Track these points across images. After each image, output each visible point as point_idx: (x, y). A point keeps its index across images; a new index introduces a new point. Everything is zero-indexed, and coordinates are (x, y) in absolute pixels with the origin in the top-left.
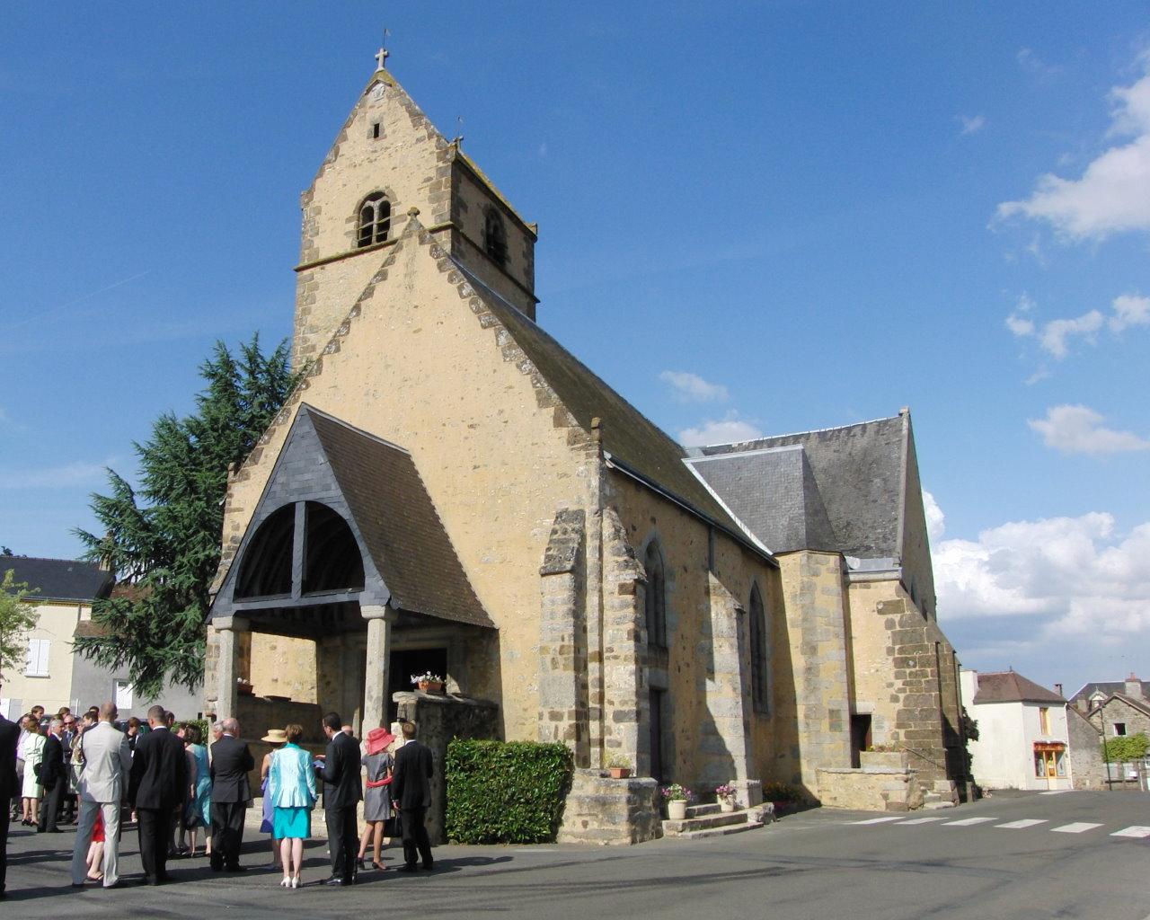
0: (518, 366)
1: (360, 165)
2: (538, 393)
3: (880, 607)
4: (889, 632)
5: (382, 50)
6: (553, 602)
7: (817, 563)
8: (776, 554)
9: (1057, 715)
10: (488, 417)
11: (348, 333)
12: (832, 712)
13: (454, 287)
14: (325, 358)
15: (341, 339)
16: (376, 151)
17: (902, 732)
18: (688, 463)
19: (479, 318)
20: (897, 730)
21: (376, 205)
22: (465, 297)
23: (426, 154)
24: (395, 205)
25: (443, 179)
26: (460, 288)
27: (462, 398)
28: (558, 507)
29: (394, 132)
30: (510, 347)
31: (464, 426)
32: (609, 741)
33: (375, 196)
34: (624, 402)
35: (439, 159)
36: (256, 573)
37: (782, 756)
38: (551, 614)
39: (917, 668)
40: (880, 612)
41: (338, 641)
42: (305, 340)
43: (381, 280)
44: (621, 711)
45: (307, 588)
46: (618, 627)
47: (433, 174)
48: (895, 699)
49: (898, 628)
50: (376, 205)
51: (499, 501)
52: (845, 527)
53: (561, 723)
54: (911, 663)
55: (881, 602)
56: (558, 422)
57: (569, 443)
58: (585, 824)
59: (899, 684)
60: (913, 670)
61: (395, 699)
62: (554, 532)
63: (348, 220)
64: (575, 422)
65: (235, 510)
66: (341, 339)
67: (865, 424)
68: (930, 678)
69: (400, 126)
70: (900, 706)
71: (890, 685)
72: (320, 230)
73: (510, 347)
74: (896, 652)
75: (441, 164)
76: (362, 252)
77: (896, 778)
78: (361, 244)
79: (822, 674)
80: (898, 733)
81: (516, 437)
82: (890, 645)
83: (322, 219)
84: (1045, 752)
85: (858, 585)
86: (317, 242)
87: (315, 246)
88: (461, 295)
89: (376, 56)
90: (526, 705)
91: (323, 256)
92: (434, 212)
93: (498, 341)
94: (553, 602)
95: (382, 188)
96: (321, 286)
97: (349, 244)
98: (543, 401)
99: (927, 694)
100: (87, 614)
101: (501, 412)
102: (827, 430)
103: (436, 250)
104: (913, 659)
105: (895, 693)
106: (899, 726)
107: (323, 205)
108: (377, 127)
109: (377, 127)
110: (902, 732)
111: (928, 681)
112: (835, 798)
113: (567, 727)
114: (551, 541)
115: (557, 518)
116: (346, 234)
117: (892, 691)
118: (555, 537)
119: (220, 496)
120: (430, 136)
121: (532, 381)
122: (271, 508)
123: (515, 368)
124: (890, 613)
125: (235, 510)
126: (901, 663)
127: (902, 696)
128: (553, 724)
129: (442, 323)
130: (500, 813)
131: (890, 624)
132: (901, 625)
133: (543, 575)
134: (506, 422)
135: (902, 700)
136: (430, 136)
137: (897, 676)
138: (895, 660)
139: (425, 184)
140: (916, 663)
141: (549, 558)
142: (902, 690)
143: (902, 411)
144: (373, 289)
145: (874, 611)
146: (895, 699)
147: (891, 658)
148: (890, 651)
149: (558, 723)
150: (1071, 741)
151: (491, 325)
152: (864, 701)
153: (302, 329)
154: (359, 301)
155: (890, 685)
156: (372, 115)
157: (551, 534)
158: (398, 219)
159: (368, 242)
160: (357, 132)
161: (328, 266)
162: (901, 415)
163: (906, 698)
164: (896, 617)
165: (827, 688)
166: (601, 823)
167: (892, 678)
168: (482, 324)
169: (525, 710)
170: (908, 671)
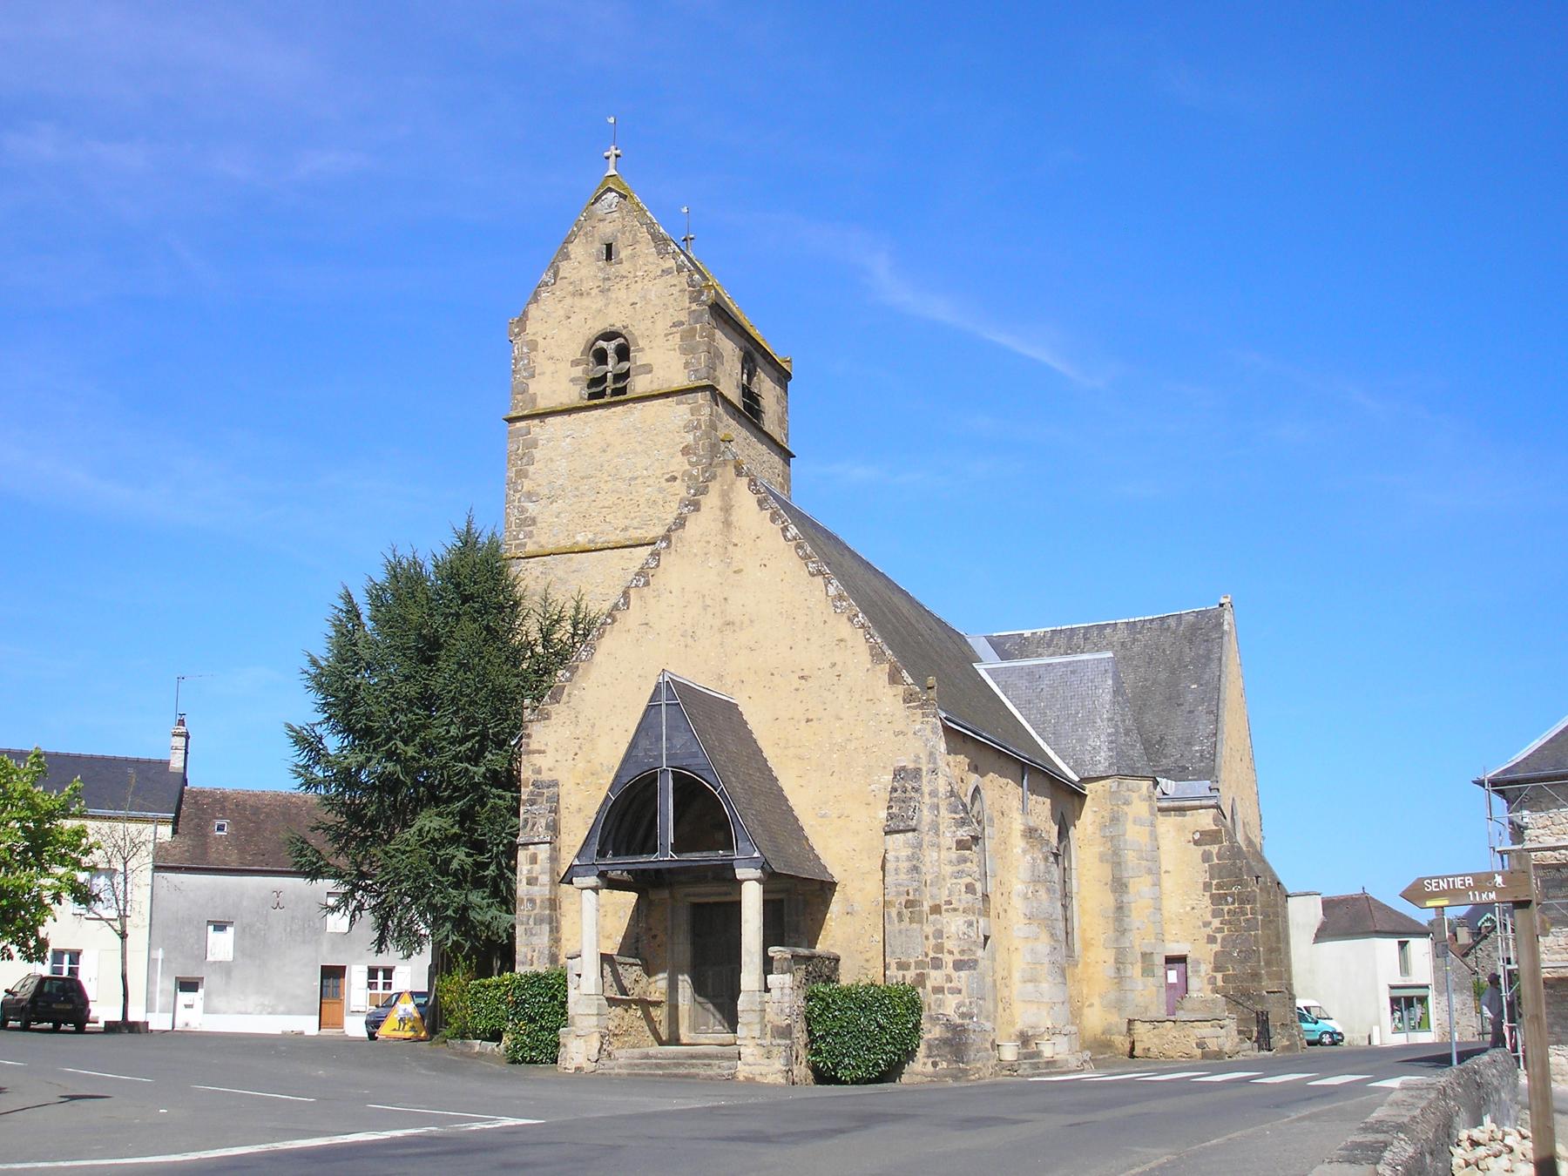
0: (849, 619)
1: (588, 294)
2: (872, 648)
3: (1197, 836)
4: (1207, 865)
5: (613, 147)
6: (897, 859)
7: (1128, 790)
8: (1085, 780)
9: (1420, 948)
10: (819, 669)
11: (658, 566)
12: (1144, 955)
13: (778, 527)
14: (632, 592)
15: (651, 572)
16: (609, 279)
17: (1219, 976)
18: (981, 669)
19: (806, 565)
20: (1215, 974)
21: (610, 347)
22: (789, 540)
23: (675, 291)
24: (634, 351)
25: (698, 326)
26: (784, 530)
27: (791, 648)
28: (896, 765)
29: (633, 256)
30: (840, 597)
31: (795, 677)
32: (949, 988)
33: (609, 336)
34: (918, 606)
35: (693, 299)
36: (725, 860)
37: (1091, 1005)
38: (896, 870)
39: (1236, 905)
40: (1196, 843)
41: (666, 894)
42: (523, 510)
43: (693, 511)
44: (961, 960)
45: (677, 848)
46: (955, 881)
47: (684, 317)
48: (1211, 939)
49: (1216, 861)
50: (610, 347)
51: (835, 756)
52: (1159, 742)
53: (909, 972)
54: (1230, 899)
55: (1197, 831)
56: (894, 678)
57: (904, 701)
58: (935, 1064)
59: (1216, 923)
60: (1231, 907)
61: (770, 954)
62: (894, 790)
63: (575, 363)
64: (910, 681)
65: (534, 752)
66: (651, 572)
67: (1181, 614)
68: (1250, 916)
69: (640, 256)
70: (1217, 947)
71: (1207, 924)
72: (537, 372)
73: (840, 597)
74: (1214, 887)
75: (694, 306)
76: (596, 407)
77: (1212, 1026)
78: (592, 396)
79: (1134, 914)
80: (1215, 978)
81: (850, 692)
82: (1207, 880)
83: (539, 358)
84: (1406, 1003)
85: (1173, 813)
86: (534, 387)
87: (531, 391)
88: (785, 537)
89: (606, 154)
90: (868, 956)
91: (543, 404)
92: (686, 365)
93: (827, 591)
94: (897, 859)
95: (618, 326)
96: (540, 442)
97: (574, 394)
98: (877, 656)
99: (1246, 933)
100: (165, 832)
101: (834, 665)
102: (1137, 619)
103: (755, 485)
104: (1232, 895)
105: (1211, 933)
106: (1217, 969)
107: (540, 340)
108: (609, 247)
109: (609, 247)
110: (1219, 976)
111: (1248, 920)
112: (1149, 1049)
113: (914, 976)
114: (891, 800)
115: (895, 775)
116: (572, 380)
117: (1209, 931)
118: (895, 795)
119: (512, 735)
120: (680, 269)
121: (865, 636)
122: (634, 772)
123: (846, 620)
124: (1206, 844)
125: (534, 752)
126: (1217, 900)
127: (1219, 936)
128: (901, 972)
129: (765, 565)
130: (880, 1045)
131: (1206, 857)
132: (1219, 859)
133: (886, 833)
134: (839, 676)
135: (1219, 940)
136: (680, 269)
137: (1215, 914)
138: (1212, 896)
139: (674, 329)
140: (1234, 899)
141: (891, 817)
142: (1220, 930)
143: (1223, 601)
144: (685, 519)
145: (1190, 842)
146: (1211, 939)
147: (1208, 894)
148: (1207, 886)
149: (905, 972)
150: (1436, 982)
151: (820, 573)
152: (1178, 942)
153: (518, 495)
154: (668, 531)
155: (1207, 924)
156: (606, 230)
157: (891, 792)
158: (642, 370)
159: (602, 394)
160: (582, 253)
161: (550, 420)
162: (1221, 605)
163: (1223, 939)
164: (1215, 849)
165: (1138, 929)
166: (949, 1062)
167: (1208, 917)
168: (809, 571)
169: (867, 961)
170: (1226, 908)
